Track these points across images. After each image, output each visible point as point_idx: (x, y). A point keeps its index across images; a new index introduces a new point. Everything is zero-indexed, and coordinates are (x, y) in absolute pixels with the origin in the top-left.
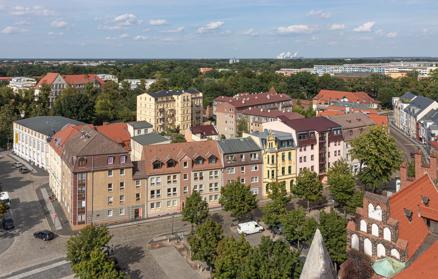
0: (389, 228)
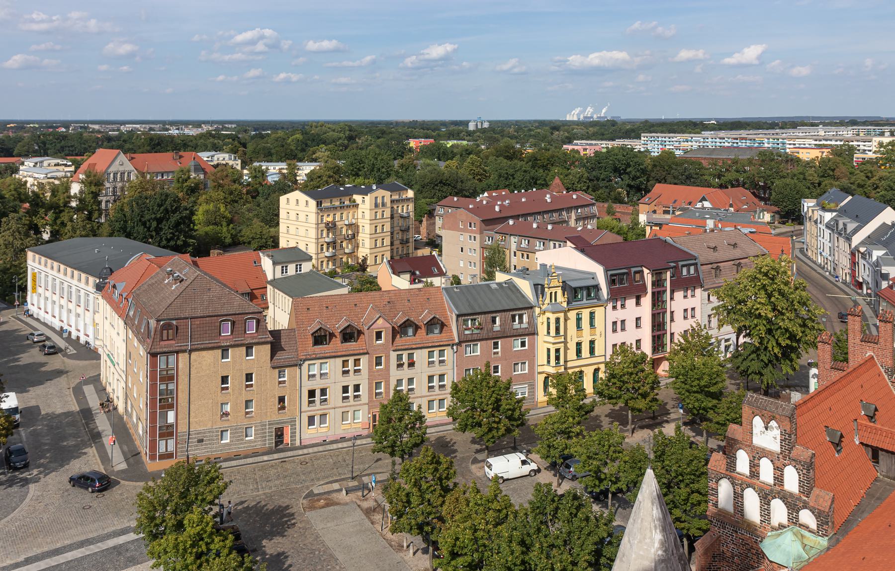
0: (795, 467)
